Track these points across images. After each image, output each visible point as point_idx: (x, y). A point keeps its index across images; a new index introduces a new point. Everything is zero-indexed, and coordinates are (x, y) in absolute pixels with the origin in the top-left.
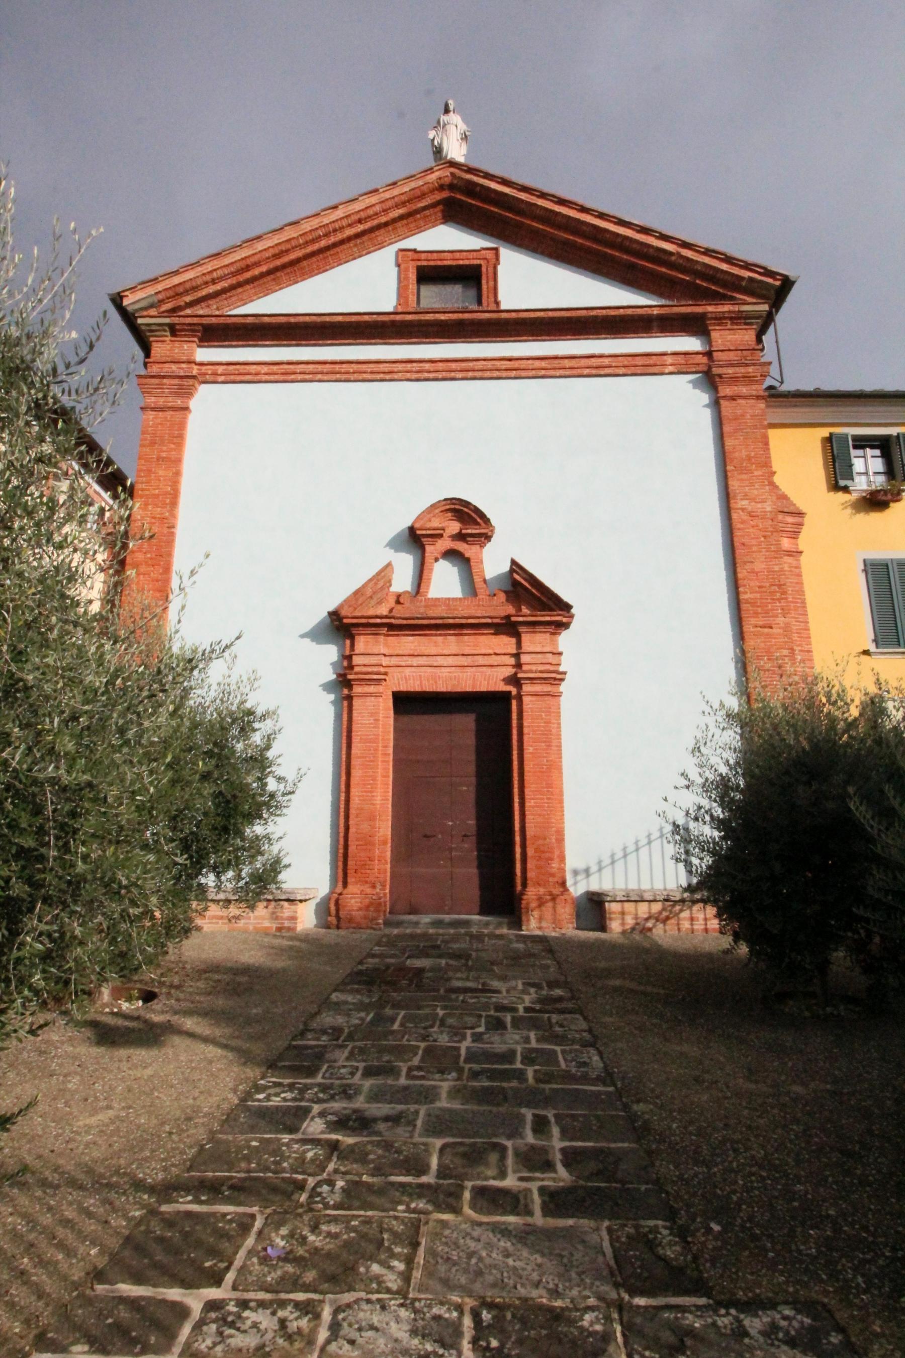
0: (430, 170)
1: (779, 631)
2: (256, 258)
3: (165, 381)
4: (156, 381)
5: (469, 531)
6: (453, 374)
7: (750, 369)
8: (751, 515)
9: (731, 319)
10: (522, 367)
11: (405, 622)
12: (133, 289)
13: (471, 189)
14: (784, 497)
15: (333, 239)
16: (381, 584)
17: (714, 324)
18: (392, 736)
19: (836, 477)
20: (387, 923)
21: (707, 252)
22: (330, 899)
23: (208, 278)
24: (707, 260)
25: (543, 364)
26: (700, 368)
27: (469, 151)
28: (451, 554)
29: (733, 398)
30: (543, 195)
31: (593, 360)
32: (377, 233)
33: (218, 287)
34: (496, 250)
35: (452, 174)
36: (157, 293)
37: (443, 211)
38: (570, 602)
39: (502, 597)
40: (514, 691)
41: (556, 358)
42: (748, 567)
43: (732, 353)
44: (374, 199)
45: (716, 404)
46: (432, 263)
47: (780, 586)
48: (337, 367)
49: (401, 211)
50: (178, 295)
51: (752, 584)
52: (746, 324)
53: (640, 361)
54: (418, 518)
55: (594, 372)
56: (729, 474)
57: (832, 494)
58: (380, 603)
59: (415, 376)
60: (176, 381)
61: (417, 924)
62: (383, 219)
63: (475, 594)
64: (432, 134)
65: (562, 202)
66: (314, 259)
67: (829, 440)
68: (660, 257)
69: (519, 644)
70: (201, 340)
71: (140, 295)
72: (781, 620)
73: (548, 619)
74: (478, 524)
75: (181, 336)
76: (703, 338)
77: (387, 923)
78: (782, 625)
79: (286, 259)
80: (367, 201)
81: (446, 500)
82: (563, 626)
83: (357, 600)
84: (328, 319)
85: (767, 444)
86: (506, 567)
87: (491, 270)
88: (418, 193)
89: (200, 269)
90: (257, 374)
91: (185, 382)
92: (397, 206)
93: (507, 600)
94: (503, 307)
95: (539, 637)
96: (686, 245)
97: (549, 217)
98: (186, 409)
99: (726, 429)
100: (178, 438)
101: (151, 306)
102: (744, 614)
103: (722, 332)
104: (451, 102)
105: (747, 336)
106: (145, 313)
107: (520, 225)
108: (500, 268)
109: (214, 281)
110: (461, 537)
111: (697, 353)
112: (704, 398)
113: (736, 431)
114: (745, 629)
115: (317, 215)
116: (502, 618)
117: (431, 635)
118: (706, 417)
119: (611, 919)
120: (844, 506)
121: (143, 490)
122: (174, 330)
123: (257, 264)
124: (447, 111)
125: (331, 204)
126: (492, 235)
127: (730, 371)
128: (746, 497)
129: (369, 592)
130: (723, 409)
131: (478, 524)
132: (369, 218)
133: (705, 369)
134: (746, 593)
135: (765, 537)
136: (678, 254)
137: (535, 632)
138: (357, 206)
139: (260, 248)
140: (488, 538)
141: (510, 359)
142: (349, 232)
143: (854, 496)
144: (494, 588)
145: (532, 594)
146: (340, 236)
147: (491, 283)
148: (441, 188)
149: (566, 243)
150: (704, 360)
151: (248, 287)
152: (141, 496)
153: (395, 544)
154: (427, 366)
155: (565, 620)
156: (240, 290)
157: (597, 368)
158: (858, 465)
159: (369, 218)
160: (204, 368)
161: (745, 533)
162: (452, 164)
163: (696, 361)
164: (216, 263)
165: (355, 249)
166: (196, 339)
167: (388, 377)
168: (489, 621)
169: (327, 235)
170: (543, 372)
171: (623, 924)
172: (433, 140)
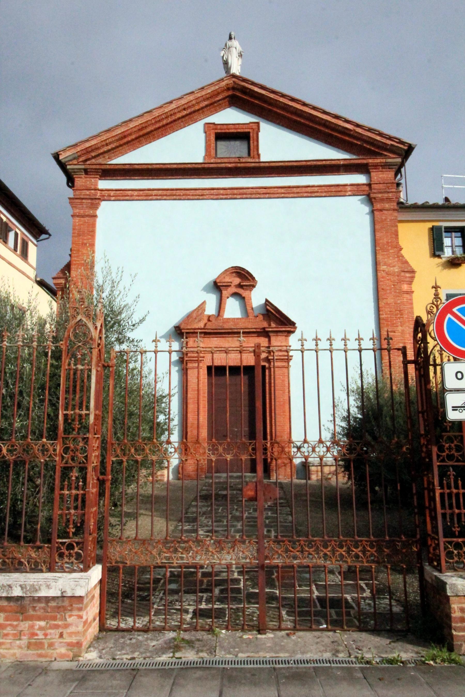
0: (222, 80)
1: (399, 334)
2: (129, 132)
3: (84, 201)
4: (79, 201)
5: (244, 284)
6: (235, 196)
7: (390, 195)
8: (388, 274)
9: (381, 166)
10: (272, 192)
11: (212, 331)
12: (64, 150)
13: (244, 90)
14: (406, 262)
15: (170, 120)
16: (200, 311)
17: (373, 169)
18: (206, 388)
19: (434, 250)
20: (206, 477)
21: (370, 130)
22: (179, 466)
23: (104, 143)
24: (369, 134)
25: (283, 191)
26: (365, 193)
27: (242, 63)
28: (235, 295)
29: (381, 210)
30: (283, 96)
31: (309, 188)
32: (193, 115)
33: (109, 147)
34: (258, 123)
35: (234, 82)
36: (77, 152)
37: (229, 101)
38: (295, 321)
39: (261, 317)
40: (267, 365)
41: (289, 187)
42: (385, 301)
43: (381, 185)
44: (191, 98)
45: (372, 212)
46: (223, 131)
47: (400, 311)
48: (174, 192)
49: (206, 103)
50: (89, 152)
51: (386, 310)
52: (389, 168)
53: (333, 189)
54: (219, 277)
55: (309, 195)
56: (377, 252)
57: (432, 259)
58: (200, 321)
59: (216, 197)
60: (89, 201)
61: (220, 477)
62: (197, 108)
63: (248, 316)
64: (222, 53)
65: (293, 100)
66: (160, 130)
67: (432, 229)
68: (345, 131)
69: (270, 341)
70: (101, 176)
71: (68, 153)
72: (400, 328)
73: (284, 329)
74: (249, 280)
75: (90, 175)
76: (367, 175)
77: (206, 477)
78: (400, 331)
79: (145, 131)
80: (188, 98)
81: (232, 267)
82: (290, 332)
83: (188, 320)
84: (169, 166)
85: (397, 235)
86: (263, 301)
87: (255, 136)
88: (216, 93)
89: (99, 138)
90: (132, 196)
91: (94, 201)
92: (204, 100)
93: (264, 319)
94: (262, 159)
95: (280, 338)
96: (358, 126)
97: (286, 108)
98: (96, 216)
99: (377, 227)
100: (92, 232)
101: (74, 159)
102: (382, 325)
103: (377, 173)
104: (232, 33)
105: (389, 175)
106: (71, 163)
107: (270, 111)
108: (260, 134)
109: (107, 145)
110: (240, 286)
111: (363, 185)
112: (366, 209)
113: (382, 228)
114: (382, 333)
115: (161, 107)
116: (261, 329)
117: (226, 337)
118: (367, 220)
119: (312, 474)
120: (438, 265)
121: (75, 261)
122: (86, 171)
123: (130, 134)
124: (230, 38)
125: (169, 100)
126: (255, 114)
127: (380, 195)
128: (385, 264)
129: (194, 315)
130: (376, 216)
131: (249, 280)
132: (189, 107)
133: (367, 193)
134: (383, 314)
135: (394, 285)
136: (354, 130)
137: (277, 336)
138: (183, 102)
139: (131, 126)
140: (254, 286)
141: (265, 188)
142: (179, 115)
143: (444, 260)
144: (256, 313)
145: (276, 316)
146: (174, 118)
147: (255, 143)
148: (228, 89)
149: (295, 121)
150: (367, 188)
151: (125, 146)
152: (75, 265)
153: (206, 289)
154: (222, 192)
155: (292, 330)
156: (121, 148)
157: (311, 193)
158: (447, 241)
159: (189, 107)
160: (103, 192)
161: (385, 284)
162: (234, 76)
163: (363, 189)
164: (109, 135)
165: (182, 124)
166: (98, 176)
167: (201, 197)
168: (255, 330)
169: (167, 117)
170: (283, 195)
171: (317, 476)
172: (223, 57)
